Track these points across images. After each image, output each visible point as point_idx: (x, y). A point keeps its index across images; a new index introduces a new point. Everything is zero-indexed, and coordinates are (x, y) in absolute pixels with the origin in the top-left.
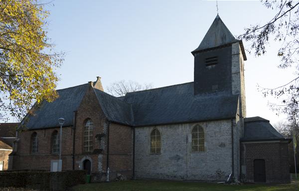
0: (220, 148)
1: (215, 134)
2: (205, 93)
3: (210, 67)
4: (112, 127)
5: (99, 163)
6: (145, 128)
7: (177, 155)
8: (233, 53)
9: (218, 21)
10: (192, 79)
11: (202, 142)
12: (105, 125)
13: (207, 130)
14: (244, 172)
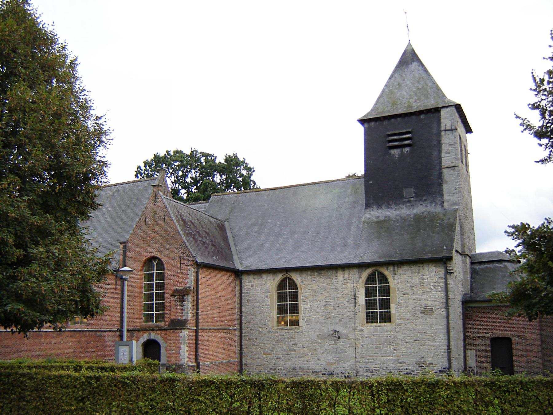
0: (420, 315)
1: (412, 289)
2: (389, 204)
3: (396, 152)
4: (203, 274)
5: (182, 346)
6: (265, 276)
7: (335, 331)
8: (443, 128)
9: (410, 58)
10: (360, 171)
11: (386, 304)
12: (192, 272)
13: (396, 281)
14: (472, 363)
